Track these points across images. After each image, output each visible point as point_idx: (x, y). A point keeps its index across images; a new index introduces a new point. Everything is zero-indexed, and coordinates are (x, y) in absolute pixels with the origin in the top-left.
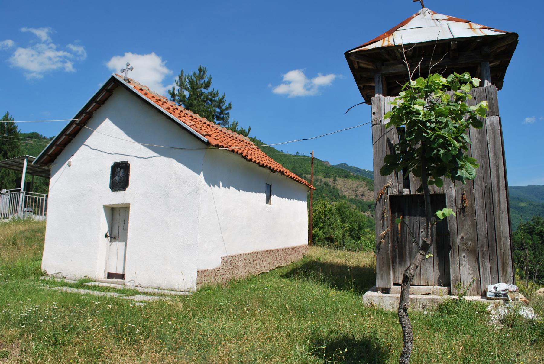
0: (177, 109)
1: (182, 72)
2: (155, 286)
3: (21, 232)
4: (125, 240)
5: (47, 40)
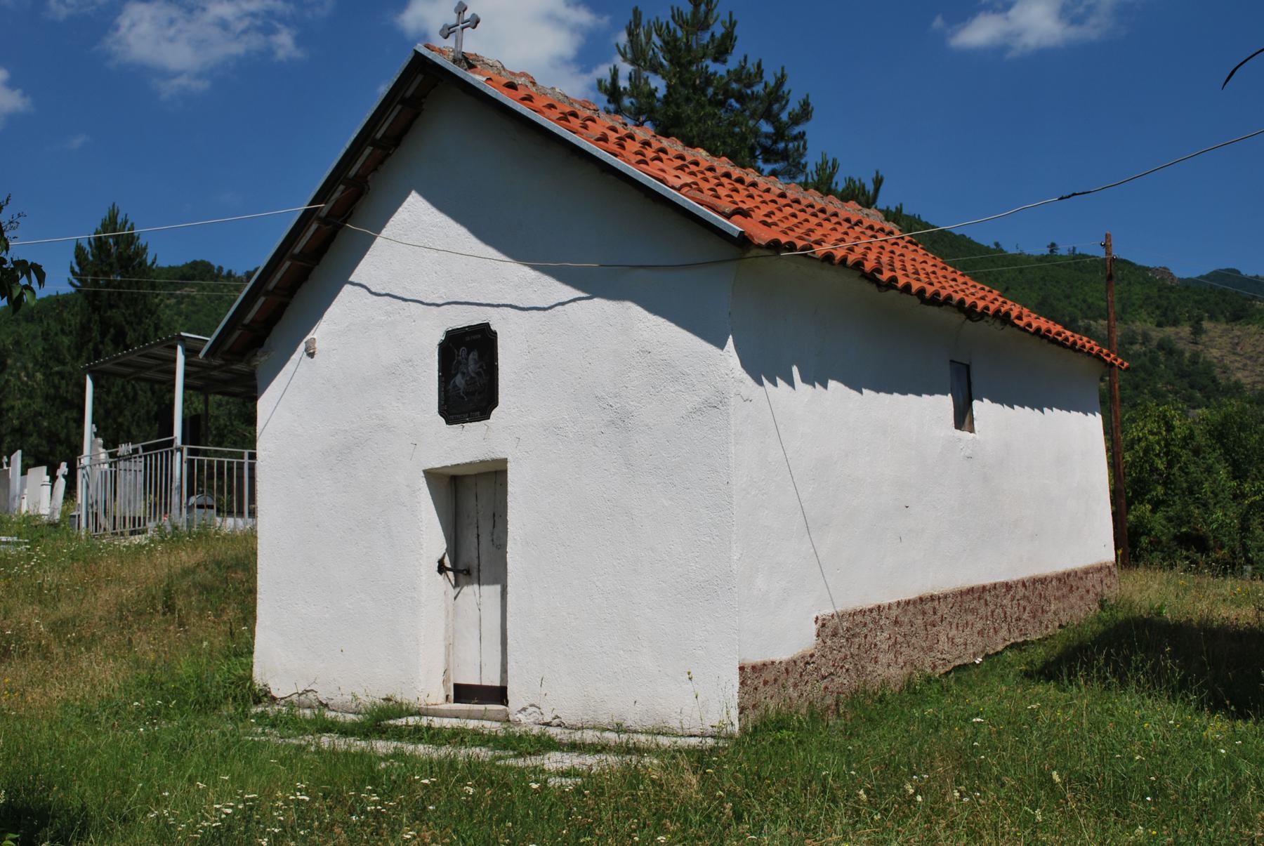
0: (631, 137)
1: (637, 13)
2: (605, 720)
3: (186, 572)
4: (500, 577)
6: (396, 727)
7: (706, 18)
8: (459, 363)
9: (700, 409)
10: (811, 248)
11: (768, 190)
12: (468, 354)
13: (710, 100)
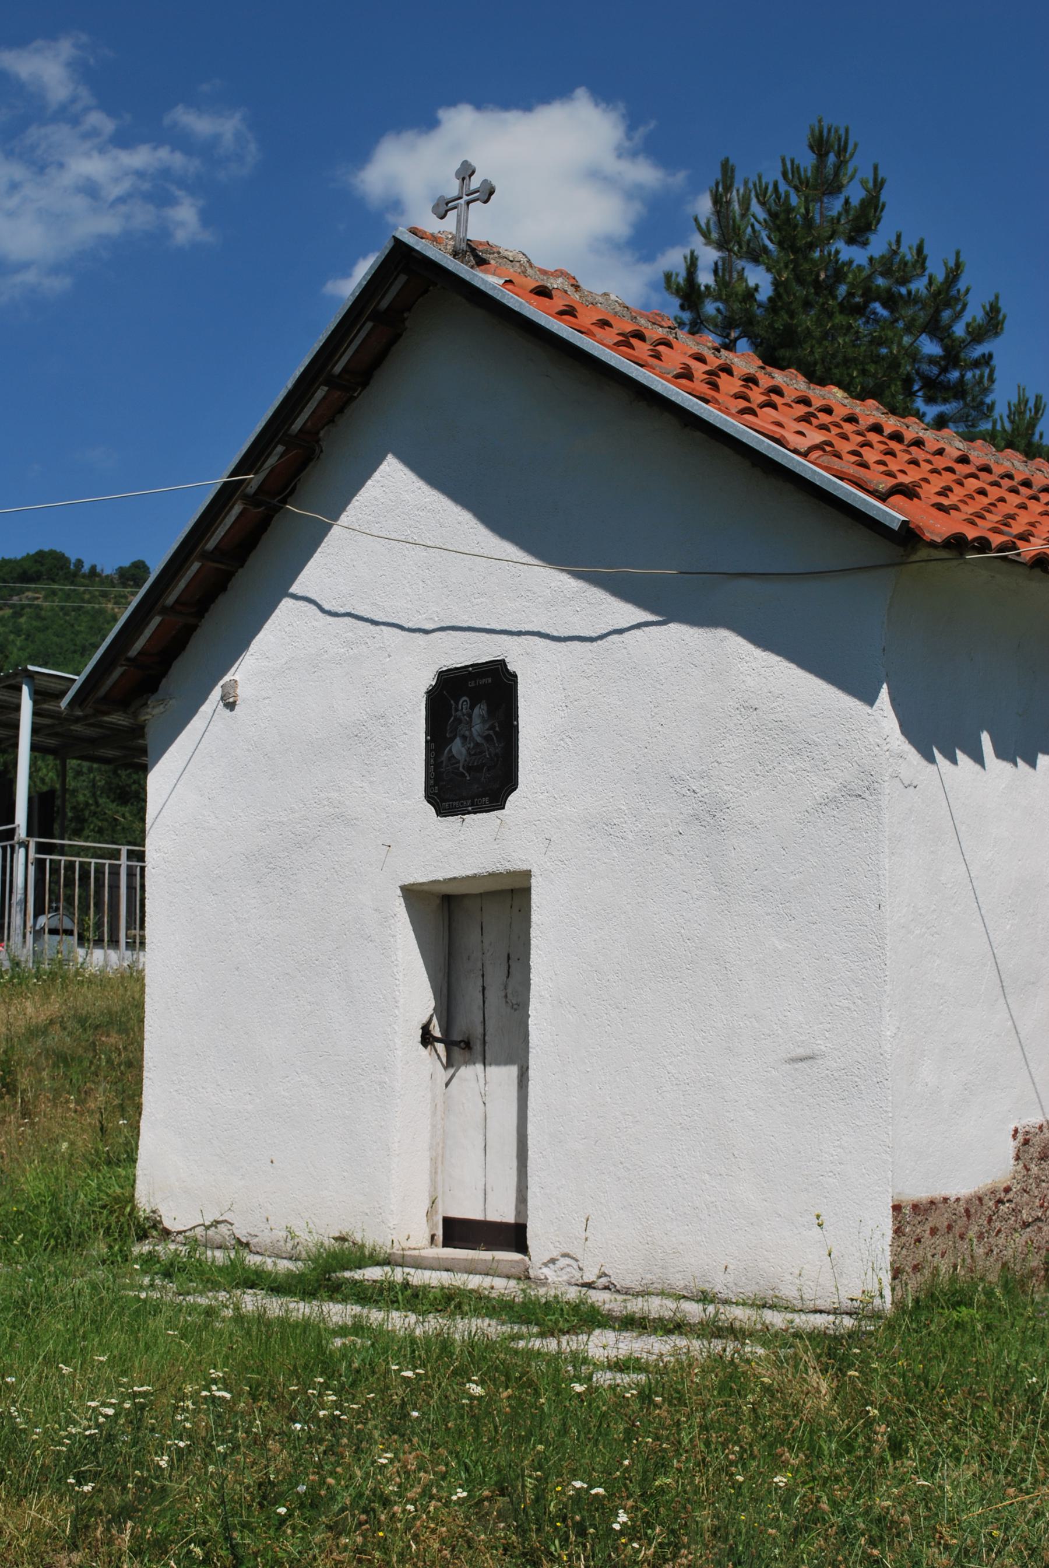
0: (727, 370)
1: (727, 171)
2: (679, 1282)
3: (34, 1032)
4: (517, 1053)
5: (74, 100)
6: (355, 1282)
7: (836, 174)
8: (459, 721)
9: (835, 800)
10: (1014, 547)
11: (940, 452)
12: (472, 708)
13: (841, 304)
